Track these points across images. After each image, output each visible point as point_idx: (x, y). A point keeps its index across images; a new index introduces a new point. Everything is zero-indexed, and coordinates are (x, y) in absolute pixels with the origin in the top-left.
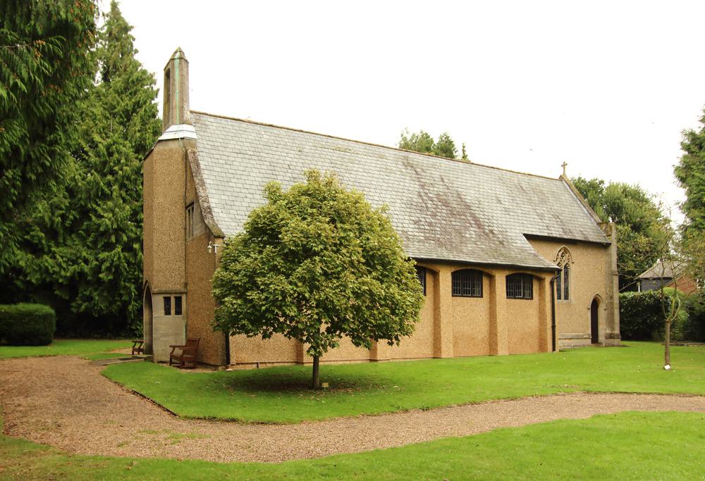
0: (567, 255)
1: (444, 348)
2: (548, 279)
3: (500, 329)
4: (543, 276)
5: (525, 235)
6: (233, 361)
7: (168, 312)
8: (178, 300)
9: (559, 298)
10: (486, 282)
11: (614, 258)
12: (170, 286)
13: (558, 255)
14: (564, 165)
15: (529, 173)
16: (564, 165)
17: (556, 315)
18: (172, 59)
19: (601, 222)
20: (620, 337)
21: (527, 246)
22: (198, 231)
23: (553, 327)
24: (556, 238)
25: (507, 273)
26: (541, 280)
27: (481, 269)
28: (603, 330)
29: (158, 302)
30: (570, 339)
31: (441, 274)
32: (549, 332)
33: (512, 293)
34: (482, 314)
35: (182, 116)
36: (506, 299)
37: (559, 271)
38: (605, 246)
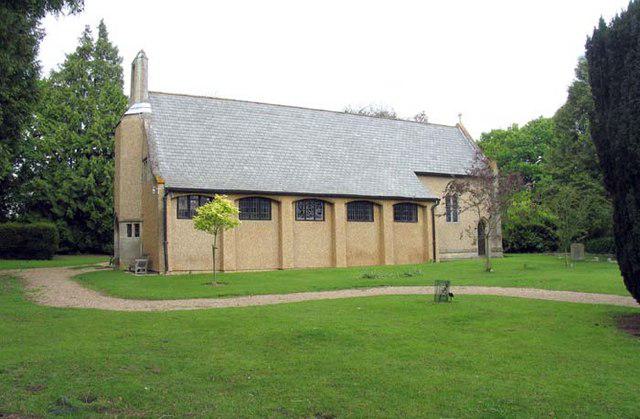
1: (338, 260)
2: (429, 206)
3: (386, 245)
4: (425, 204)
5: (416, 173)
6: (170, 269)
7: (130, 235)
8: (137, 226)
12: (131, 217)
14: (460, 115)
15: (377, 108)
16: (460, 115)
18: (137, 58)
22: (149, 177)
25: (393, 203)
26: (424, 208)
29: (123, 227)
32: (431, 247)
33: (301, 214)
35: (142, 97)
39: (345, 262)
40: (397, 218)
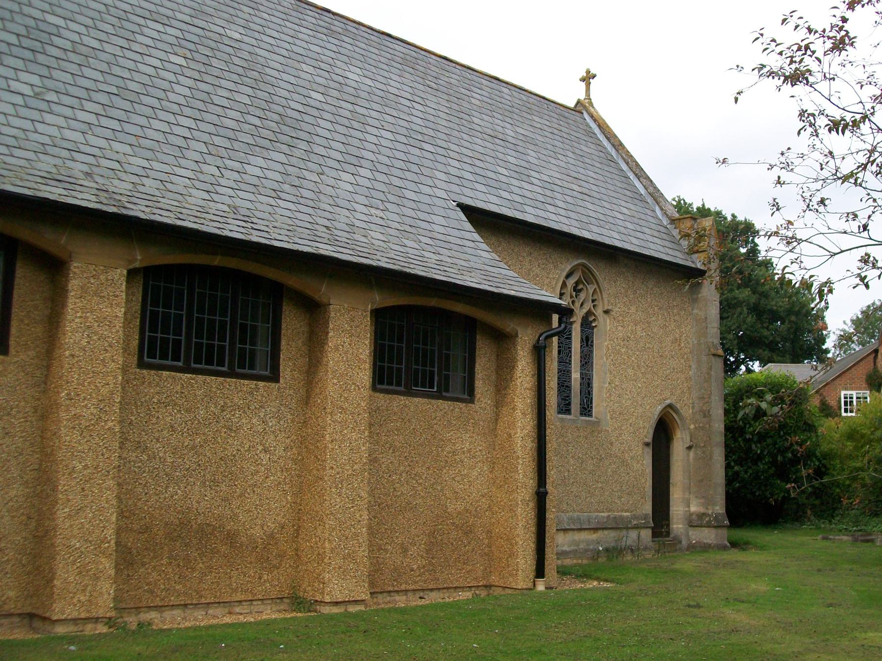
0: (591, 289)
1: (65, 575)
2: (525, 338)
4: (509, 324)
9: (565, 408)
10: (292, 324)
11: (714, 311)
13: (564, 285)
16: (588, 78)
17: (549, 455)
19: (677, 215)
20: (727, 522)
21: (468, 235)
23: (541, 498)
24: (545, 526)
25: (379, 299)
26: (502, 339)
27: (270, 273)
28: (683, 504)
30: (595, 530)
31: (75, 267)
34: (270, 440)
36: (366, 392)
37: (566, 313)
38: (692, 275)
39: (107, 590)
40: (385, 377)
